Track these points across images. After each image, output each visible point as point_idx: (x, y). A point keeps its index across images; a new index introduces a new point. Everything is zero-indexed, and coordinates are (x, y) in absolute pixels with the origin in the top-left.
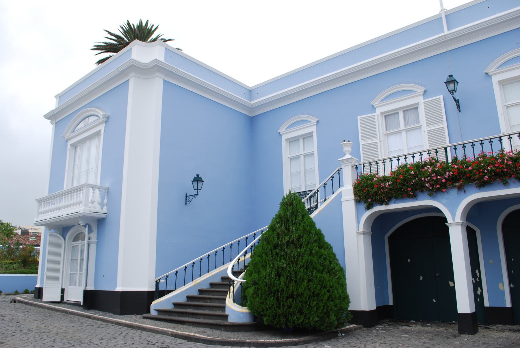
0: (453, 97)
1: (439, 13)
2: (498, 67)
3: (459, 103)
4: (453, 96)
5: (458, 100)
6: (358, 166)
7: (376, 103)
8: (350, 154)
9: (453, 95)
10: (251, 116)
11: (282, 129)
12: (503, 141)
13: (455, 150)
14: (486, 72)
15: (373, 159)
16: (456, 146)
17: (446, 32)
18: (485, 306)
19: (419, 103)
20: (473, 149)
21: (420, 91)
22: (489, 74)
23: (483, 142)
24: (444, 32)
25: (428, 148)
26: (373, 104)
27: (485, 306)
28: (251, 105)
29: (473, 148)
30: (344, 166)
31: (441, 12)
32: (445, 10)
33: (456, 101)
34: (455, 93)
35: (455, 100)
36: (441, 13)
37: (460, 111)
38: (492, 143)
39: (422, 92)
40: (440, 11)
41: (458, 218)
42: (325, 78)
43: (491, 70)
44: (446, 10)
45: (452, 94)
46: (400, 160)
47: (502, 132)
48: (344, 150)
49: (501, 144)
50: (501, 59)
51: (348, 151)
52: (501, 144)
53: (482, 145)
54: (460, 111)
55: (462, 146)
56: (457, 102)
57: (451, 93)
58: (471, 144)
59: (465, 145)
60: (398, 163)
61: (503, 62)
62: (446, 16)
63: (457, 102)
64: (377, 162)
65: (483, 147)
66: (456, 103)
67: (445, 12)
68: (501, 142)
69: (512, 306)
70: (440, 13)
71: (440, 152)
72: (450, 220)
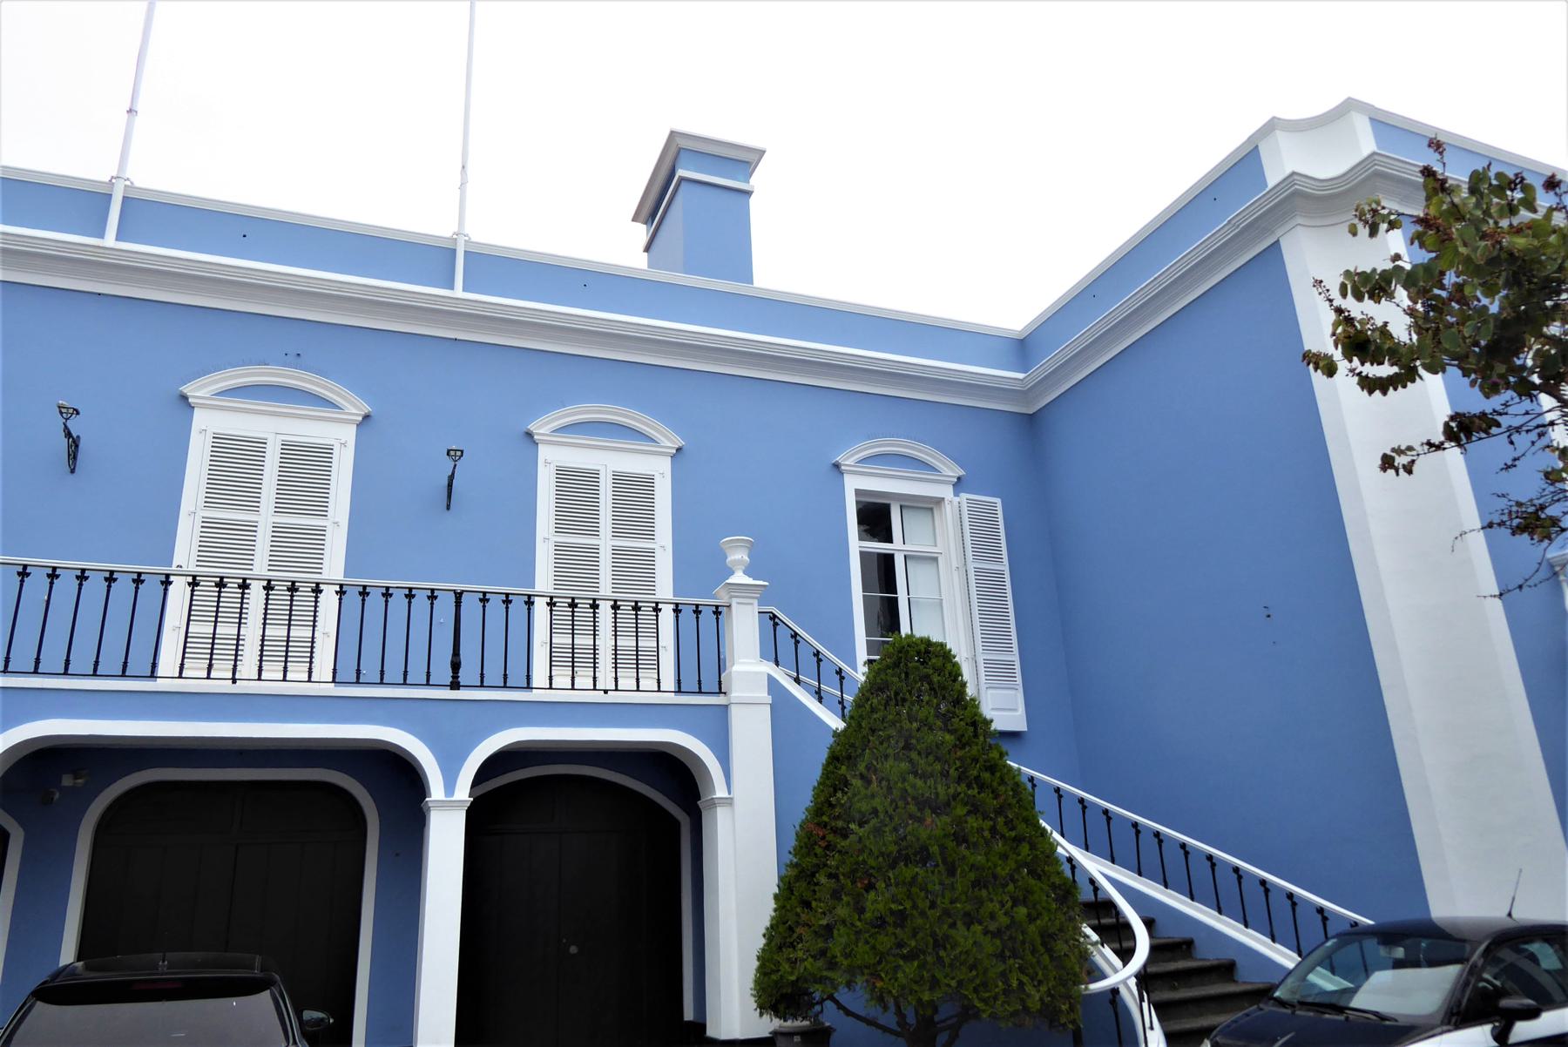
0: (63, 426)
1: (107, 179)
2: (219, 393)
3: (77, 446)
4: (64, 424)
5: (78, 437)
6: (511, 597)
7: (197, 390)
8: (745, 573)
9: (67, 419)
10: (1031, 412)
11: (205, 386)
12: (322, 597)
13: (81, 581)
14: (185, 391)
15: (233, 573)
16: (435, 591)
17: (459, 292)
18: (686, 1019)
19: (943, 499)
20: (432, 608)
21: (354, 411)
22: (190, 400)
23: (487, 597)
24: (101, 235)
25: (193, 568)
26: (535, 429)
27: (686, 1019)
28: (1020, 382)
29: (109, 587)
30: (738, 603)
31: (114, 181)
32: (128, 183)
33: (71, 440)
34: (74, 416)
35: (68, 434)
36: (113, 184)
37: (73, 471)
38: (55, 581)
39: (357, 415)
40: (112, 177)
41: (463, 793)
42: (249, 272)
43: (848, 460)
44: (470, 239)
45: (64, 415)
46: (59, 579)
47: (176, 562)
48: (727, 561)
49: (529, 613)
50: (229, 374)
51: (740, 562)
52: (529, 613)
53: (23, 578)
54: (73, 471)
55: (526, 598)
56: (74, 444)
57: (61, 413)
58: (481, 596)
59: (322, 587)
60: (48, 585)
61: (237, 384)
62: (124, 197)
63: (74, 444)
64: (194, 577)
65: (366, 602)
66: (69, 447)
67: (125, 186)
68: (529, 609)
69: (1308, 981)
70: (110, 181)
71: (202, 586)
72: (436, 791)
